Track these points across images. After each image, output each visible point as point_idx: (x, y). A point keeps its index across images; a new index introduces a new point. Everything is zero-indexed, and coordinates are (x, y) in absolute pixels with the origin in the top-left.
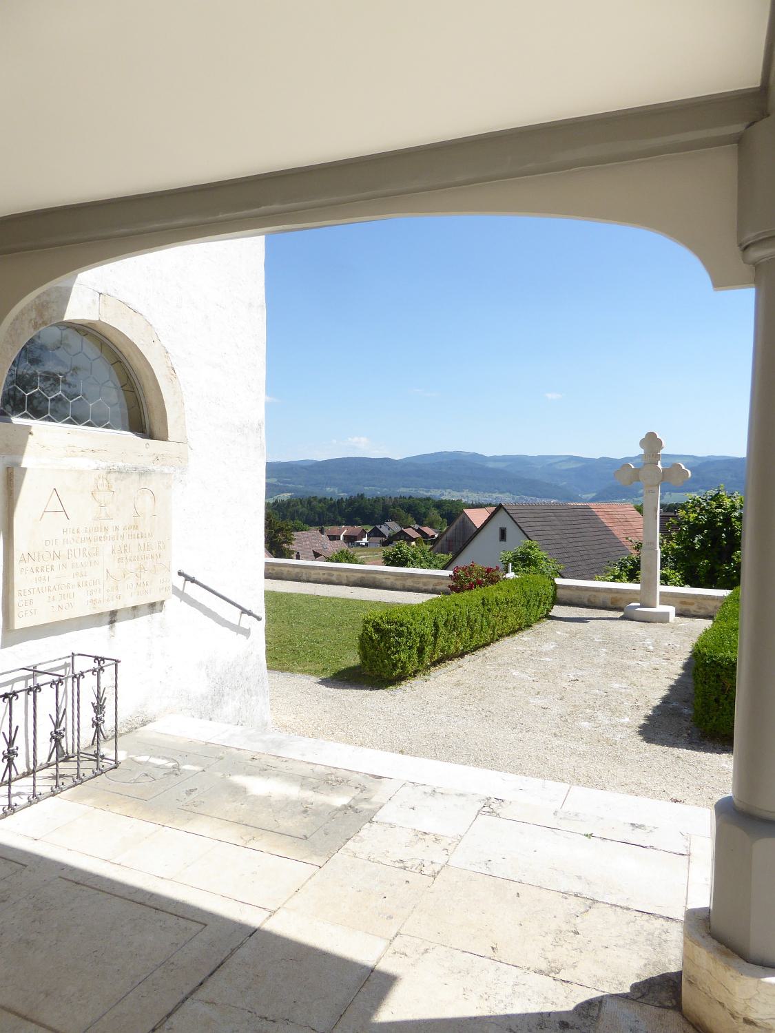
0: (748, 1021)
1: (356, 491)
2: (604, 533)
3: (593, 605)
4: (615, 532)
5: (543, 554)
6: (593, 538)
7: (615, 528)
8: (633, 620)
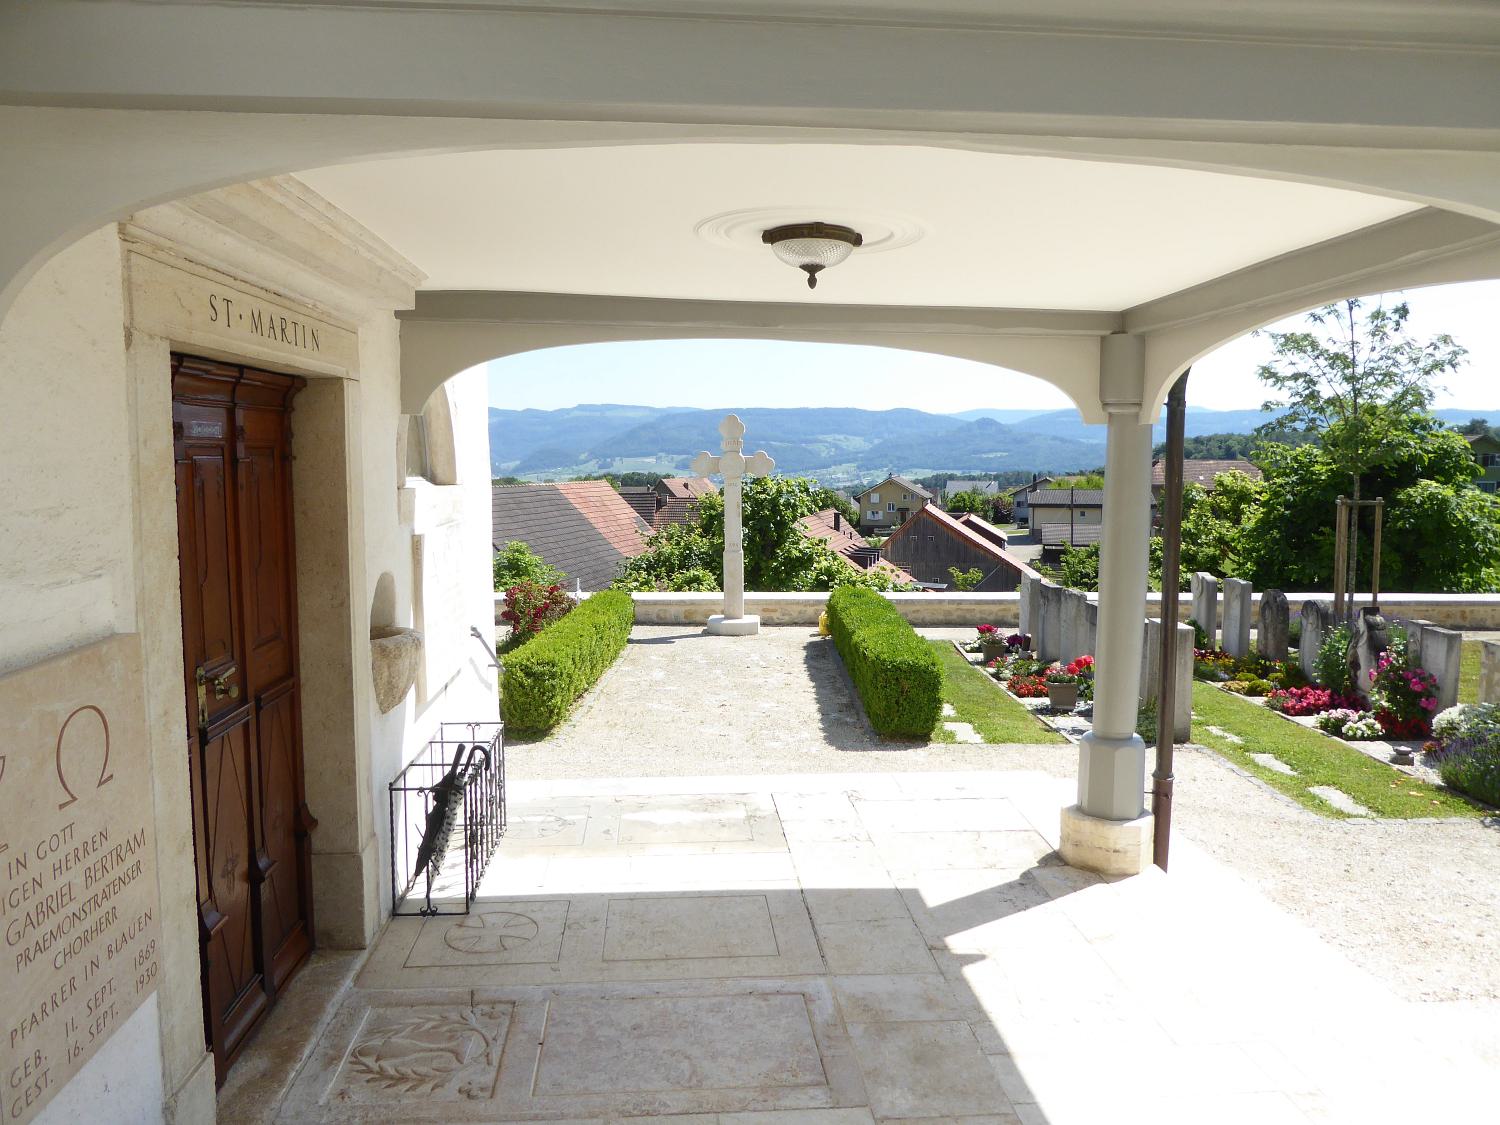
0: (1115, 851)
2: (578, 522)
4: (592, 521)
5: (537, 559)
6: (566, 530)
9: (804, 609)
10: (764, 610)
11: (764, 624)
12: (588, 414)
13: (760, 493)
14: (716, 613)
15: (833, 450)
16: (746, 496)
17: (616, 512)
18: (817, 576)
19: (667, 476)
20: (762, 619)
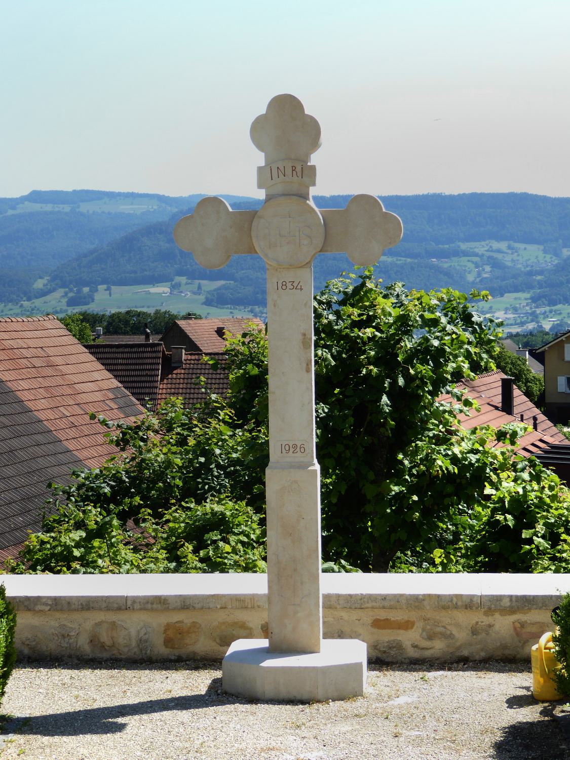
1: (525, 192)
3: (105, 655)
7: (24, 385)
8: (252, 699)
9: (486, 620)
10: (378, 624)
11: (378, 662)
12: (48, 208)
13: (361, 325)
14: (250, 636)
15: (488, 268)
16: (325, 333)
17: (75, 378)
18: (492, 516)
19: (188, 316)
20: (373, 647)
